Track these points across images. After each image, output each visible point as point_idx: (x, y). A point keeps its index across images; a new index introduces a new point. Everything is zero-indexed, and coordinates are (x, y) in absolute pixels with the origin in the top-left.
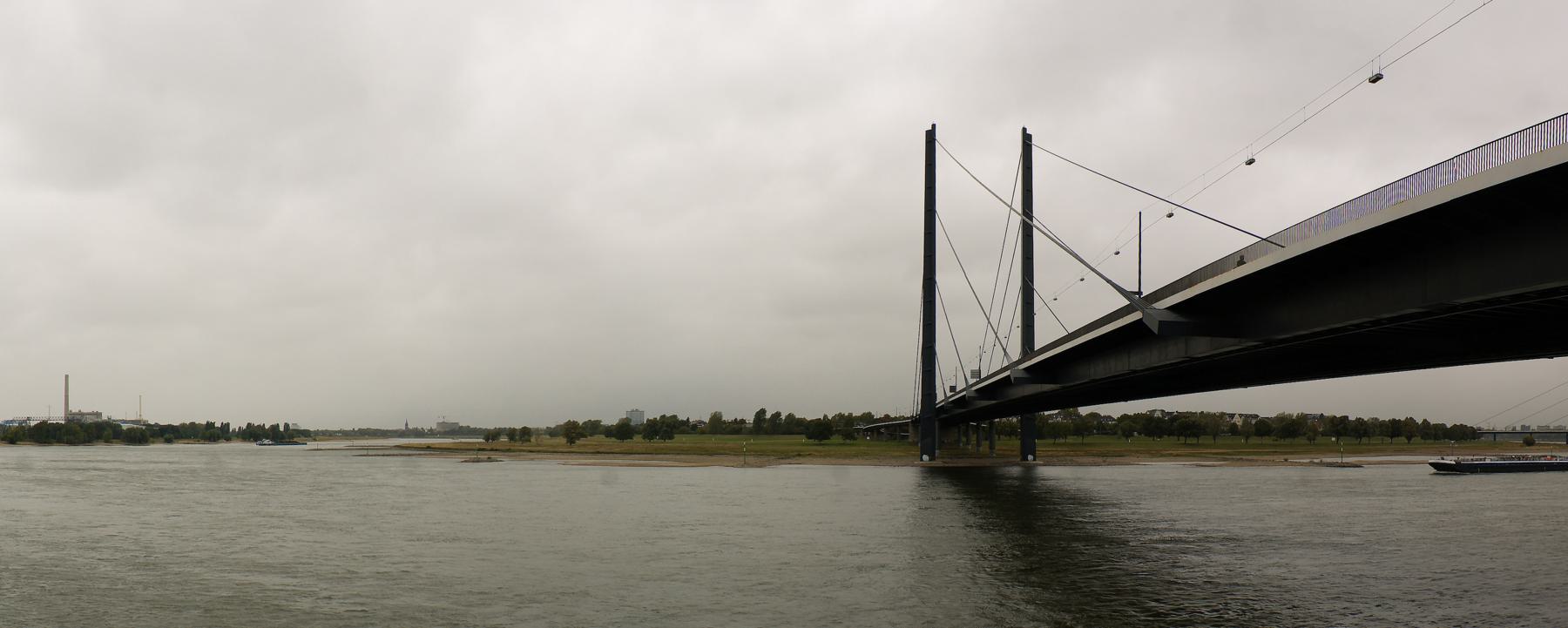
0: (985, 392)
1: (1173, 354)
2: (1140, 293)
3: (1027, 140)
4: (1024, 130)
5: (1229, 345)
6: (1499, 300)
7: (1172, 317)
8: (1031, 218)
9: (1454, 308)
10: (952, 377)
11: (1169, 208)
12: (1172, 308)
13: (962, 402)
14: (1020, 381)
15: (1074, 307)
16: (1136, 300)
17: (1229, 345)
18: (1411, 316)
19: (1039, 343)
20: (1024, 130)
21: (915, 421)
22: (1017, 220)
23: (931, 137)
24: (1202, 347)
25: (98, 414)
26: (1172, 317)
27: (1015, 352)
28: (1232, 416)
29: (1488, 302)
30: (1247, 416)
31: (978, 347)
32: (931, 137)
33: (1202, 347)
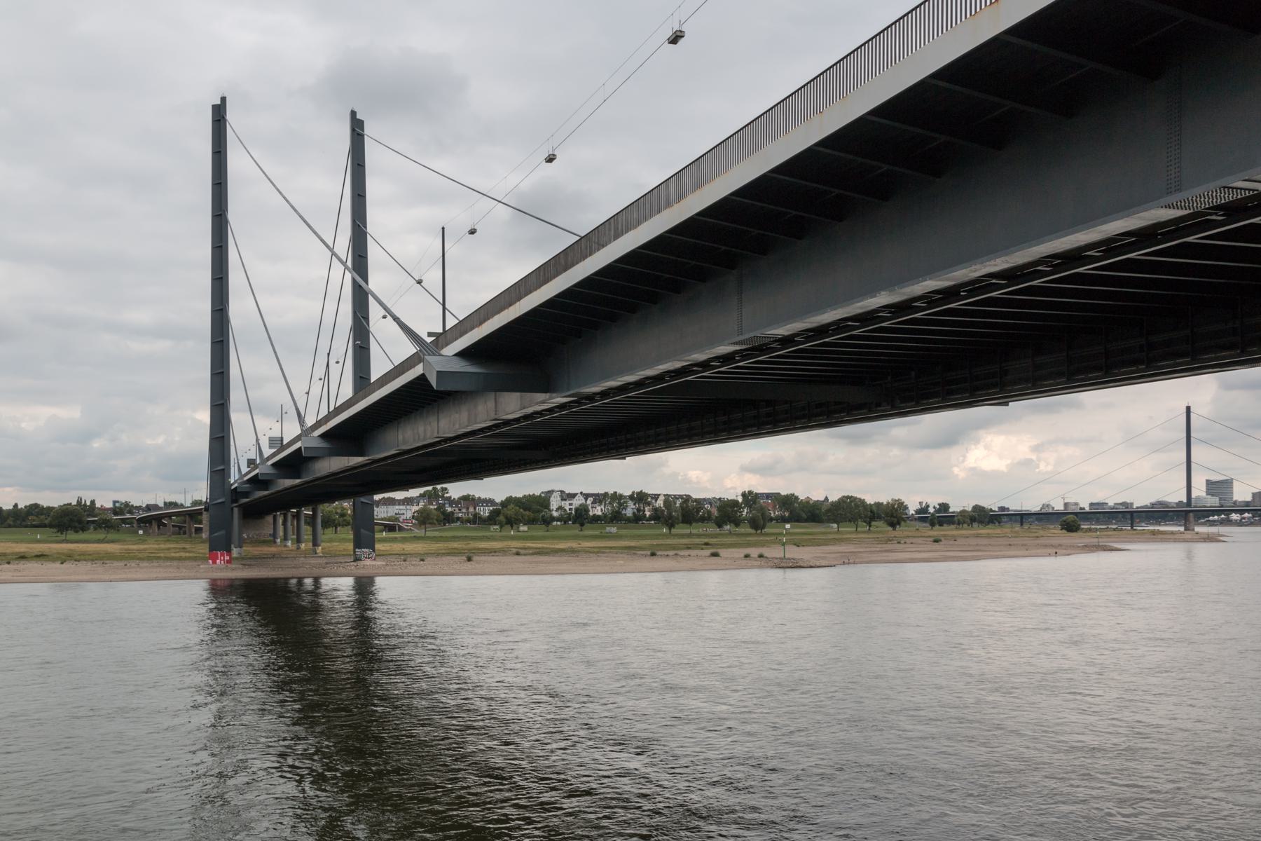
9: (591, 398)
13: (294, 463)
23: (219, 114)
32: (219, 114)
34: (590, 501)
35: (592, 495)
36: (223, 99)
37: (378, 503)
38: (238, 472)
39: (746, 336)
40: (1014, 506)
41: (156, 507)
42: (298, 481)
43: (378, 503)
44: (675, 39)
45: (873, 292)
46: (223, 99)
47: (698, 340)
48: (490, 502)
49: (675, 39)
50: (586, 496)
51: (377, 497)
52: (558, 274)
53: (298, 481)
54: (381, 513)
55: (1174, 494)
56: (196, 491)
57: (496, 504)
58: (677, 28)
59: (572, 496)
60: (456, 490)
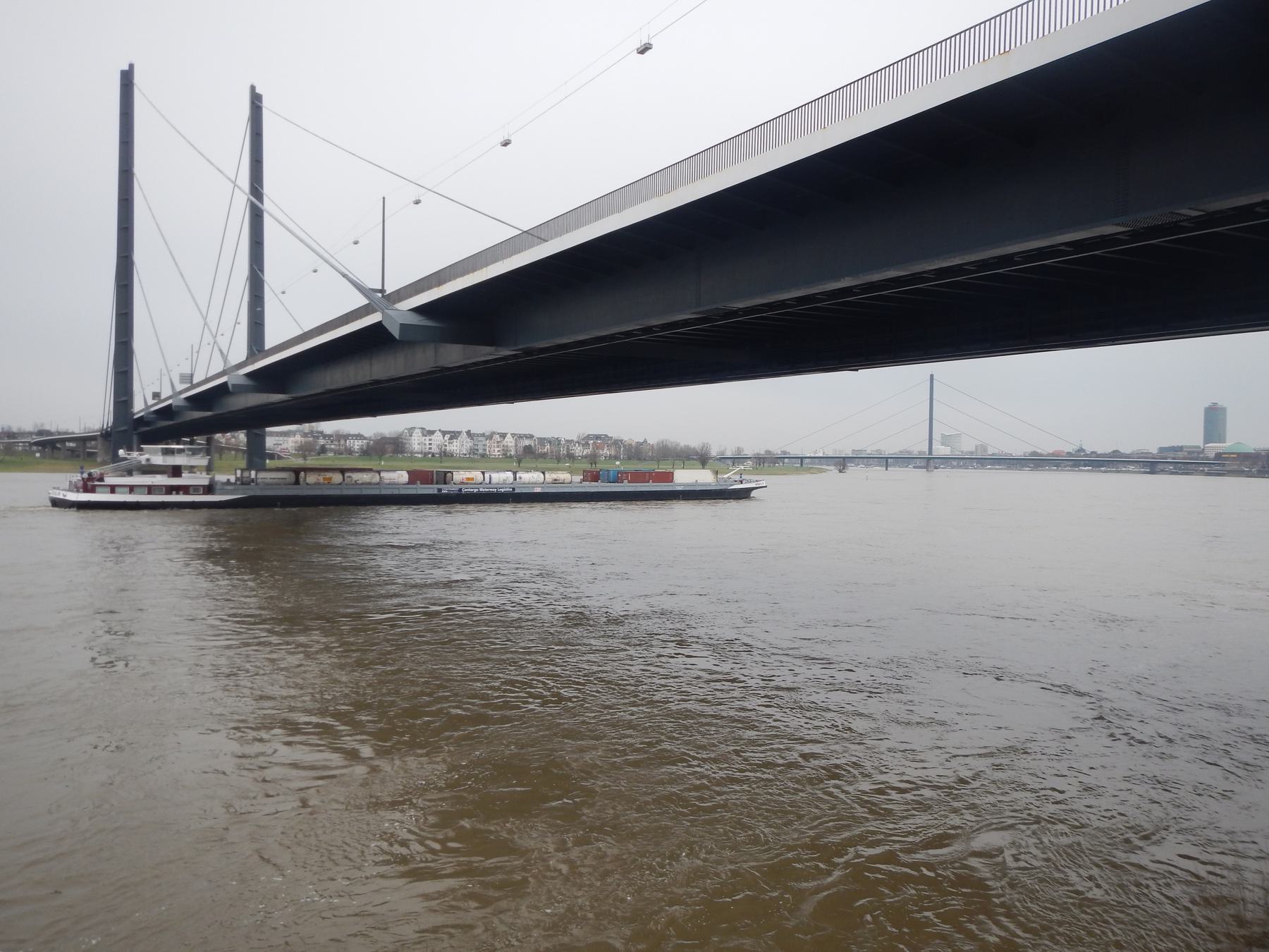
0: (199, 401)
1: (421, 361)
2: (382, 291)
3: (256, 103)
4: (253, 88)
5: (484, 353)
6: (783, 304)
7: (415, 320)
8: (261, 200)
9: (735, 313)
10: (155, 384)
11: (415, 193)
12: (419, 310)
13: (167, 412)
14: (239, 389)
15: (307, 308)
16: (382, 298)
17: (484, 353)
18: (686, 323)
19: (269, 344)
20: (253, 88)
21: (106, 435)
22: (242, 199)
23: (127, 80)
24: (454, 355)
25: (678, 445)
26: (415, 320)
27: (239, 352)
28: (503, 436)
29: (770, 306)
30: (521, 437)
31: (190, 346)
32: (127, 80)
33: (454, 355)
34: (447, 437)
35: (449, 432)
36: (131, 66)
37: (272, 434)
38: (138, 406)
39: (701, 309)
40: (795, 451)
41: (48, 433)
42: (209, 413)
43: (272, 434)
44: (644, 50)
45: (836, 278)
46: (131, 66)
47: (749, 291)
48: (359, 437)
49: (644, 50)
50: (444, 433)
51: (268, 429)
52: (357, 319)
53: (209, 413)
54: (270, 442)
55: (919, 446)
56: (90, 411)
57: (365, 438)
58: (645, 41)
59: (431, 433)
60: (329, 427)
